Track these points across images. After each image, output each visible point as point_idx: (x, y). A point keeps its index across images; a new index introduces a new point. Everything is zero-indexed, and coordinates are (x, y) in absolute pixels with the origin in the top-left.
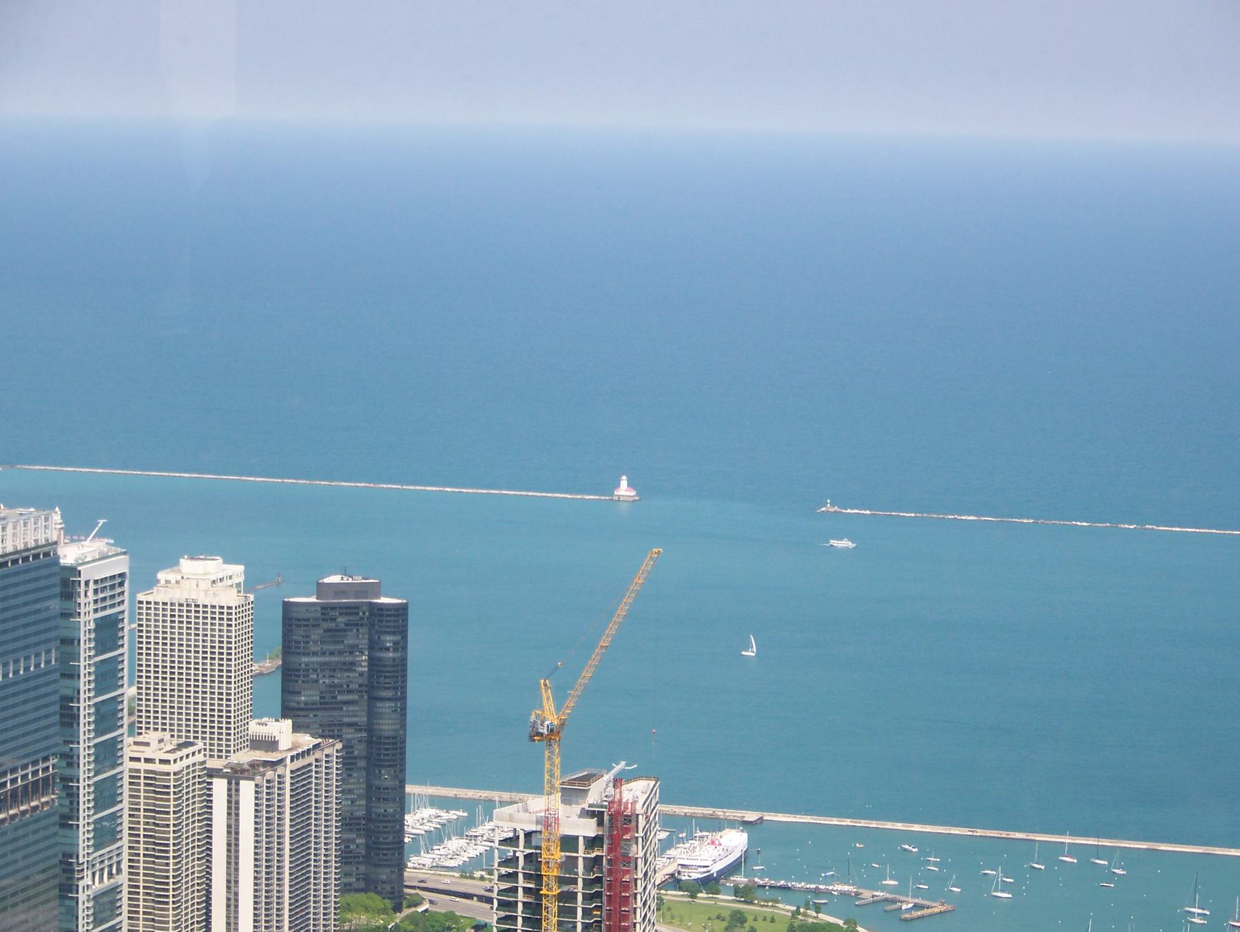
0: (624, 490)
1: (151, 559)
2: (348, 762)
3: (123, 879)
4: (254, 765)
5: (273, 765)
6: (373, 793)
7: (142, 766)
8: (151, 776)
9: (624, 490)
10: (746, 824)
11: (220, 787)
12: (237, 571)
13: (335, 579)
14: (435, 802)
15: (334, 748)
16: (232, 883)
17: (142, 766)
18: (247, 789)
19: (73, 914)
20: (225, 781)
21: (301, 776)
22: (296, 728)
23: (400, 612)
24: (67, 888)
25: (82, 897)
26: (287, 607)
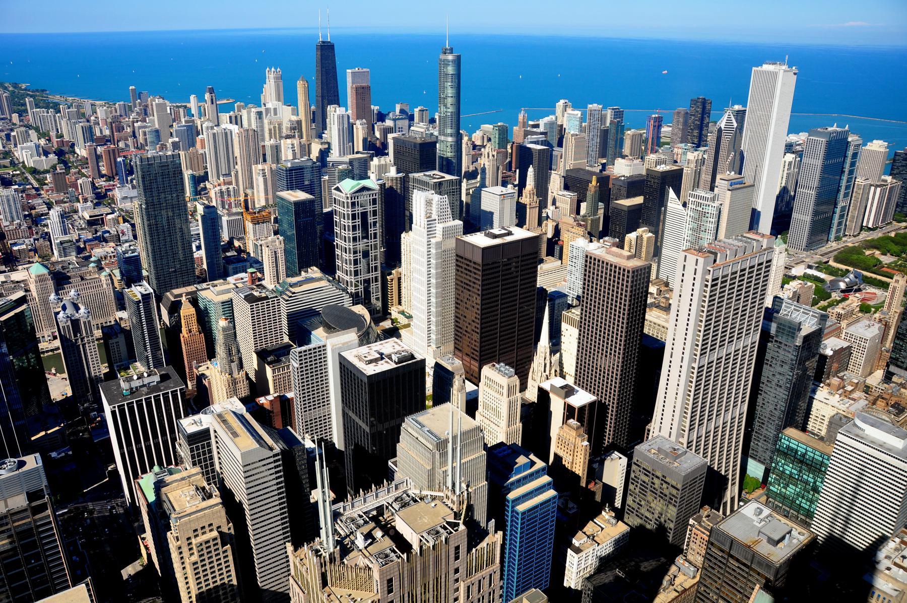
1: (868, 139)
11: (873, 188)
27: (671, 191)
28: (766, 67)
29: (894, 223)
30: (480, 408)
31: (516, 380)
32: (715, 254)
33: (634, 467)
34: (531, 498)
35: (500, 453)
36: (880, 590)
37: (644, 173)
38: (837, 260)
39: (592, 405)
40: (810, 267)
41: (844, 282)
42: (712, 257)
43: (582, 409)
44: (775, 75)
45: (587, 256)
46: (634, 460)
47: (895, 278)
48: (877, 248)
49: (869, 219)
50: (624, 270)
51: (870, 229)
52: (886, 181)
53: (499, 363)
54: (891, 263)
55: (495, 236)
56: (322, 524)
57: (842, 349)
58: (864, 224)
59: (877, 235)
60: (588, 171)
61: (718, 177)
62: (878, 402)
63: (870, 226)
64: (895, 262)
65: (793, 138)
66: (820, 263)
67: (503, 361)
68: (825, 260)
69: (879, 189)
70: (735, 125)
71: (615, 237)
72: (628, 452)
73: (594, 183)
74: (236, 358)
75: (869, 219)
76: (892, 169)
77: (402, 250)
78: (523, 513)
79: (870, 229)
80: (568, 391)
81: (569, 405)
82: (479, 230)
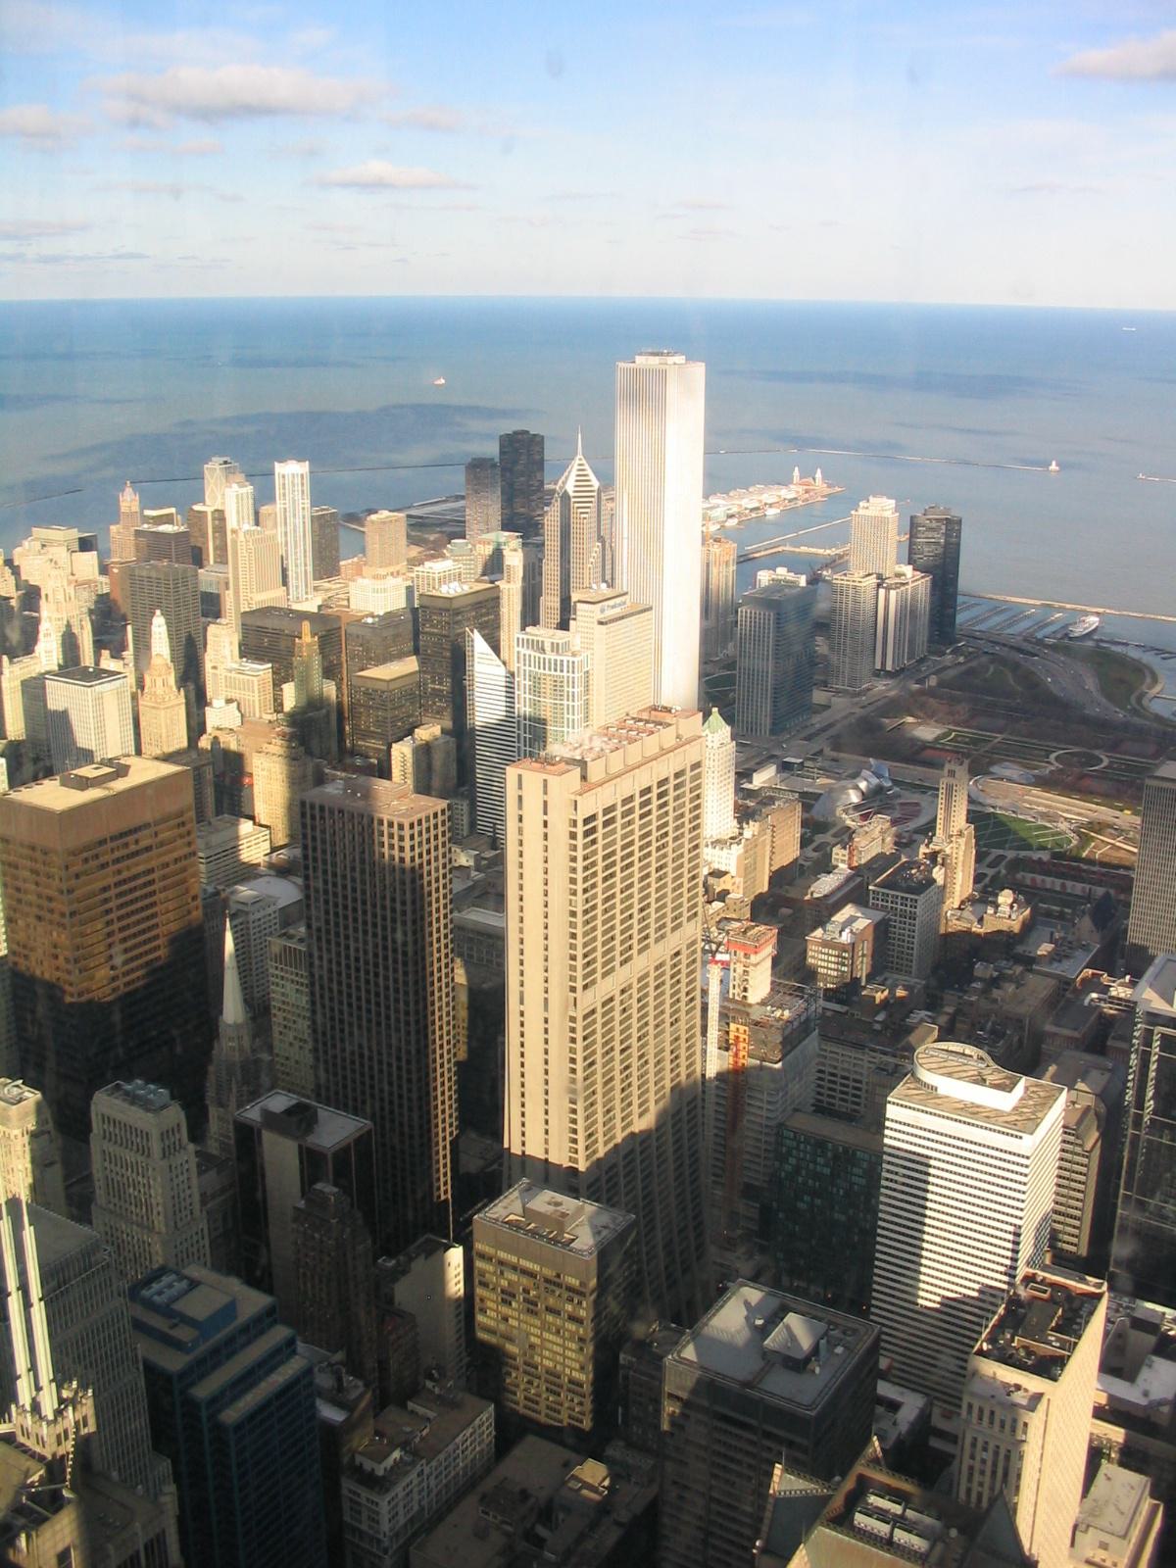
8: (855, 587)
11: (882, 592)
18: (893, 593)
28: (641, 361)
30: (100, 1194)
31: (175, 1115)
33: (479, 1264)
34: (253, 1385)
35: (160, 1293)
36: (973, 1394)
39: (362, 1141)
41: (857, 788)
42: (577, 771)
43: (342, 1155)
46: (479, 1246)
47: (947, 767)
50: (322, 808)
53: (129, 1080)
55: (84, 784)
56: (39, 1312)
62: (958, 1025)
63: (889, 668)
67: (139, 1076)
70: (596, 484)
72: (466, 1241)
73: (307, 638)
74: (698, 1002)
76: (911, 552)
78: (239, 1427)
80: (300, 1119)
81: (308, 1149)
82: (49, 773)
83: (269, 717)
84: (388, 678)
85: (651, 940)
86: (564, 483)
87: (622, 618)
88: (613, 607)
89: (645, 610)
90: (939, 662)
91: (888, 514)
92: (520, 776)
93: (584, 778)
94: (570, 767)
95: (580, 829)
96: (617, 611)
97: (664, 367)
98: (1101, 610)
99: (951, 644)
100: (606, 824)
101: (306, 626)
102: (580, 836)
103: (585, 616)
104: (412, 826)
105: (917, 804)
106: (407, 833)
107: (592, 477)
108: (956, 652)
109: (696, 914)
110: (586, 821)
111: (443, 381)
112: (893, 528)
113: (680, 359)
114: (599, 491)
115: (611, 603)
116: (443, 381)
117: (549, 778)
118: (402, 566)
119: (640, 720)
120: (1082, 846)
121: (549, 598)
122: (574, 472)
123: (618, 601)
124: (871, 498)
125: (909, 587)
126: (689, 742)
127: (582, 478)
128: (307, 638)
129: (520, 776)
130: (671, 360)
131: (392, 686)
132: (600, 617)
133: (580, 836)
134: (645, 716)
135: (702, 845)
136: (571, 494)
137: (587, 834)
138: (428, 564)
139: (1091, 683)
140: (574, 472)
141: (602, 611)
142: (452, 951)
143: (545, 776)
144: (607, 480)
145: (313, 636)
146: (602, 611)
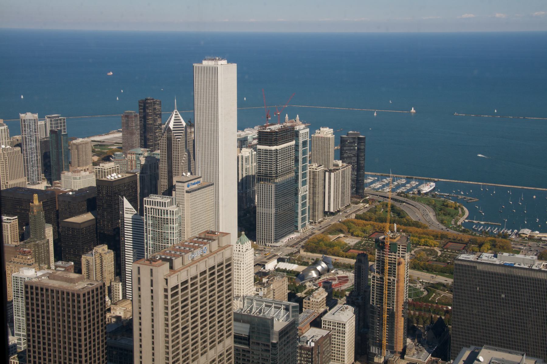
0: (413, 110)
1: (314, 127)
2: (353, 169)
3: (308, 192)
4: (334, 169)
5: (337, 169)
6: (341, 266)
7: (312, 170)
8: (314, 172)
9: (413, 110)
10: (434, 181)
11: (327, 174)
12: (332, 130)
13: (351, 132)
14: (372, 176)
15: (350, 166)
16: (329, 192)
17: (312, 170)
18: (332, 174)
19: (298, 198)
20: (213, 251)
21: (343, 172)
22: (343, 162)
23: (364, 139)
24: (296, 194)
25: (299, 196)
26: (341, 137)
27: (126, 201)
28: (205, 63)
29: (353, 205)
32: (171, 261)
37: (94, 185)
38: (307, 248)
40: (280, 260)
42: (167, 265)
44: (215, 70)
45: (26, 287)
48: (341, 231)
49: (329, 204)
50: (73, 295)
51: (332, 214)
52: (337, 165)
54: (357, 244)
57: (323, 338)
58: (326, 210)
59: (341, 217)
60: (29, 189)
61: (175, 179)
63: (332, 210)
64: (360, 243)
65: (243, 134)
66: (291, 254)
68: (295, 250)
69: (332, 174)
71: (68, 260)
73: (36, 202)
75: (329, 204)
77: (8, 283)
79: (332, 214)
83: (16, 244)
84: (80, 222)
85: (226, 354)
86: (168, 124)
87: (199, 189)
88: (194, 184)
89: (210, 185)
90: (357, 207)
91: (330, 136)
92: (139, 268)
93: (171, 267)
94: (164, 262)
95: (170, 293)
96: (196, 186)
97: (216, 66)
98: (436, 180)
99: (362, 198)
100: (183, 290)
101: (36, 196)
102: (169, 296)
103: (181, 188)
104: (84, 295)
105: (347, 277)
106: (82, 299)
107: (182, 120)
108: (366, 202)
109: (230, 334)
110: (172, 289)
111: (111, 73)
112: (332, 143)
113: (224, 62)
114: (186, 127)
115: (193, 182)
116: (111, 73)
117: (141, 266)
118: (90, 166)
119: (200, 238)
120: (429, 295)
121: (162, 180)
122: (173, 118)
123: (196, 181)
124: (321, 129)
125: (340, 171)
126: (224, 248)
127: (177, 121)
128: (36, 202)
129: (139, 268)
130: (220, 62)
131: (82, 226)
132: (186, 189)
133: (169, 296)
134: (203, 236)
135: (233, 299)
136: (172, 129)
137: (172, 296)
138: (101, 165)
139: (432, 215)
140: (173, 118)
141: (188, 186)
142: (106, 359)
143: (151, 267)
144: (191, 124)
145: (39, 202)
146: (188, 186)
